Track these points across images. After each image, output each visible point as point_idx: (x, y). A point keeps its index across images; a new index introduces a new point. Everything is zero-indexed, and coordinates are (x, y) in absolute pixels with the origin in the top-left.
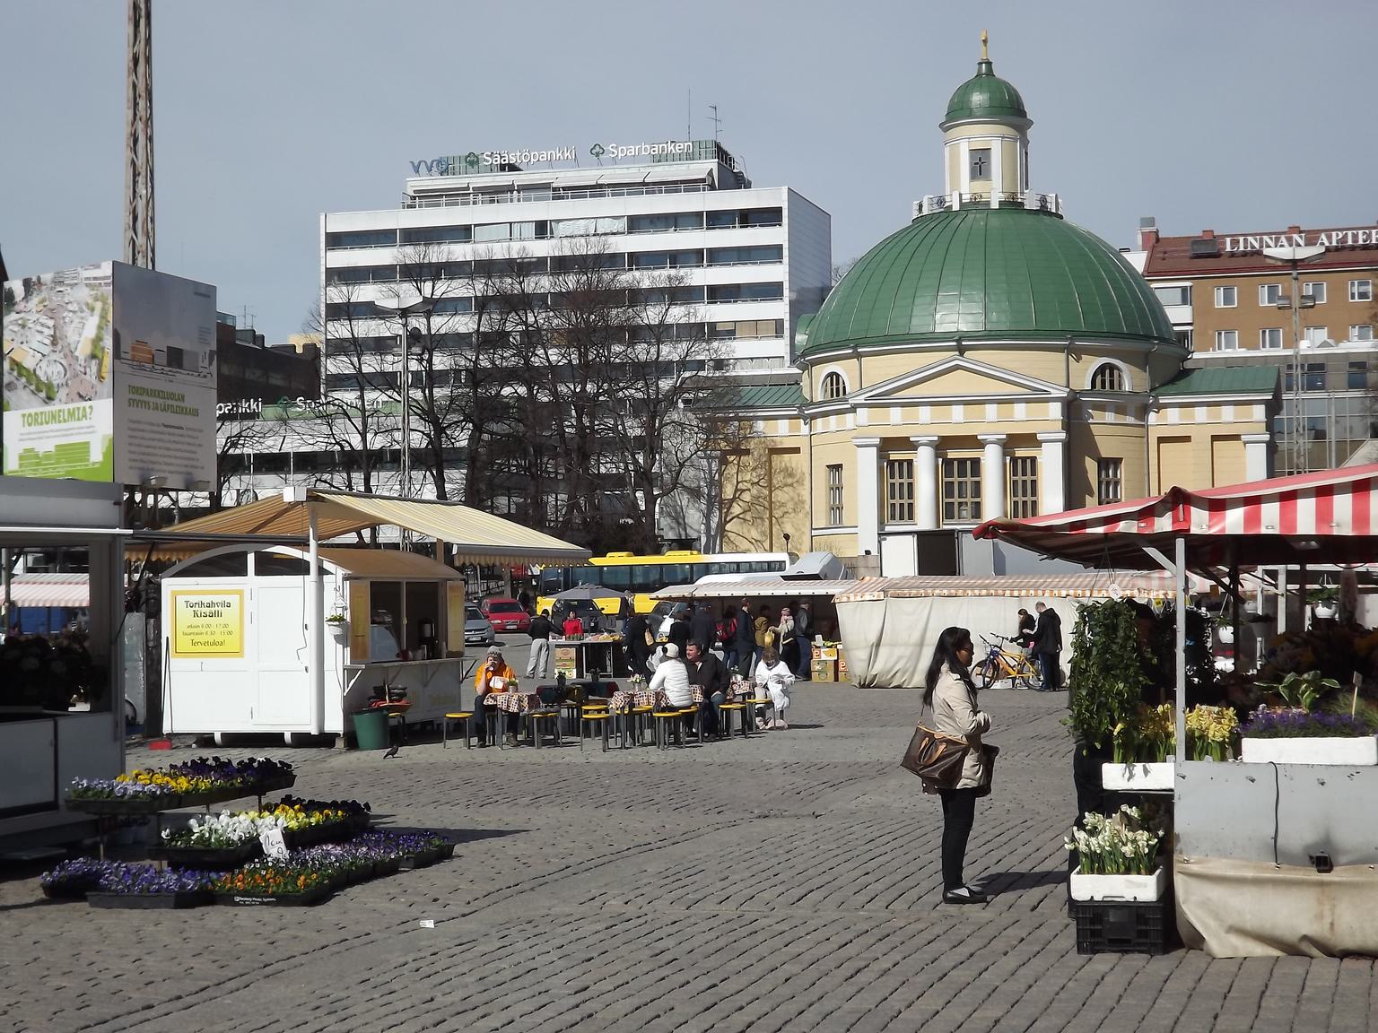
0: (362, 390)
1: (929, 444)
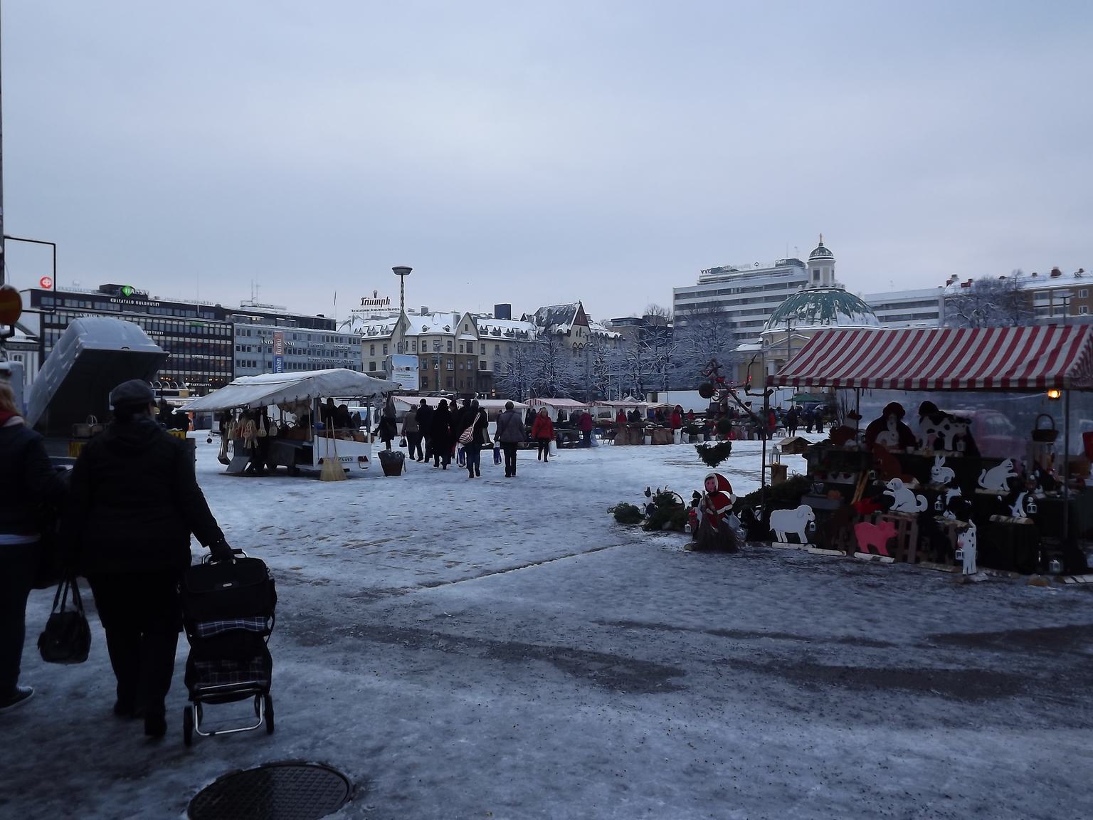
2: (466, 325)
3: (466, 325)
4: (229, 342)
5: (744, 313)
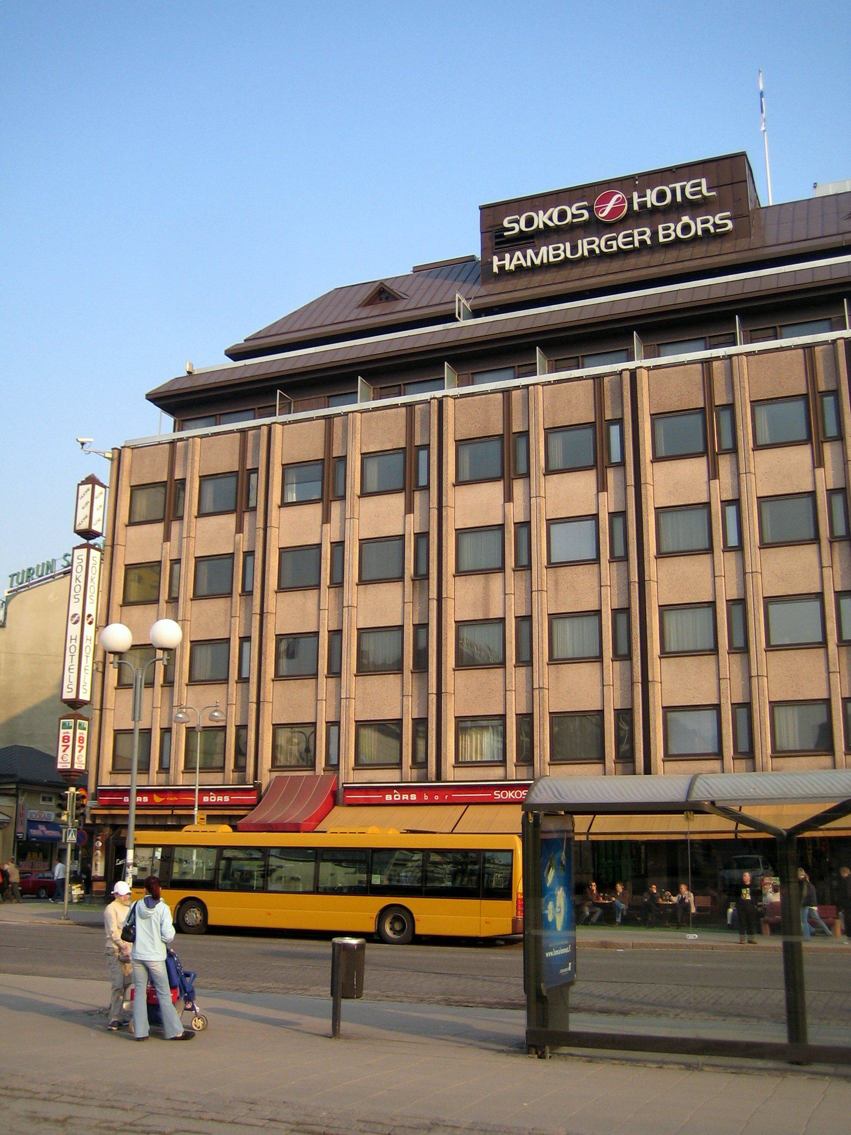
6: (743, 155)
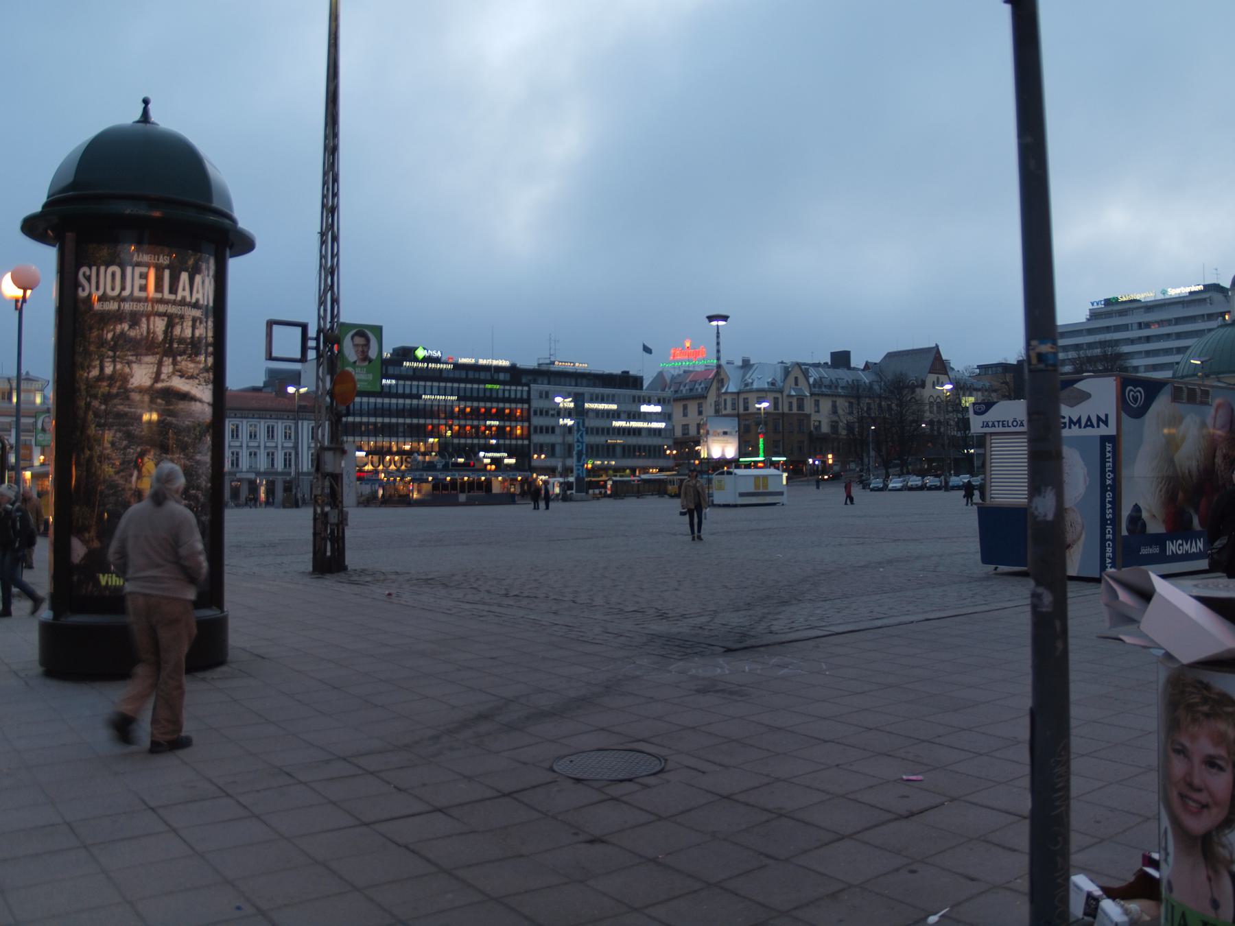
0: (411, 394)
1: (783, 387)
2: (796, 379)
3: (796, 379)
4: (526, 406)
5: (1148, 353)
6: (831, 353)
